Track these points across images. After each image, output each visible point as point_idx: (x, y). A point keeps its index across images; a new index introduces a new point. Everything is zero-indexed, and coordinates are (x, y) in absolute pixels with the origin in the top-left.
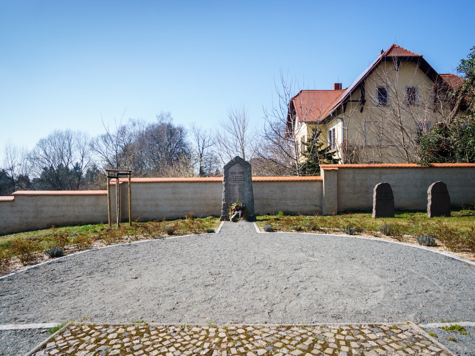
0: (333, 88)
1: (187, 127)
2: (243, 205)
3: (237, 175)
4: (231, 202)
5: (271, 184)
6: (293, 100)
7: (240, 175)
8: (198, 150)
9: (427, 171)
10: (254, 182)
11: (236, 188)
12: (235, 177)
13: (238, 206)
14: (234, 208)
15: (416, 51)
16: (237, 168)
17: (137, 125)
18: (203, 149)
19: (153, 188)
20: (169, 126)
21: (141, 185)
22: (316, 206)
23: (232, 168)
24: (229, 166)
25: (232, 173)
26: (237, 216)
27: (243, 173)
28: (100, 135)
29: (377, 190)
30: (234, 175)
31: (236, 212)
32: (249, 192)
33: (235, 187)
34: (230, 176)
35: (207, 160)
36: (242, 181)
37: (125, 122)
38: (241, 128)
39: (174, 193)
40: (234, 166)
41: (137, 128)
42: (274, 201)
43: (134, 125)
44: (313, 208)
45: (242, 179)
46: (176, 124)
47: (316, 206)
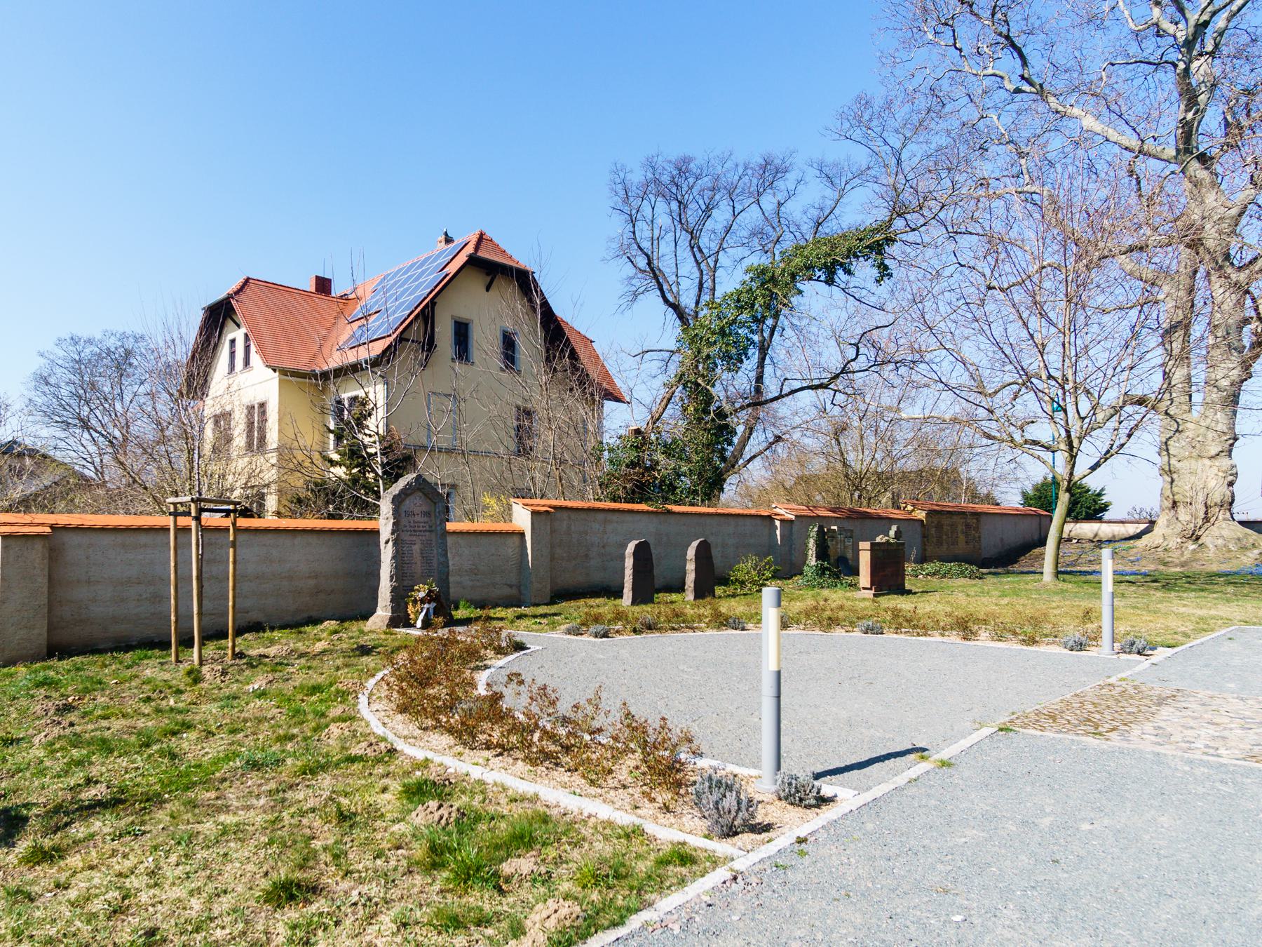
0: (310, 286)
3: (418, 518)
9: (662, 518)
15: (521, 257)
16: (418, 502)
19: (145, 546)
21: (107, 539)
22: (511, 586)
27: (428, 514)
29: (634, 554)
34: (404, 521)
40: (412, 497)
44: (507, 591)
47: (511, 586)
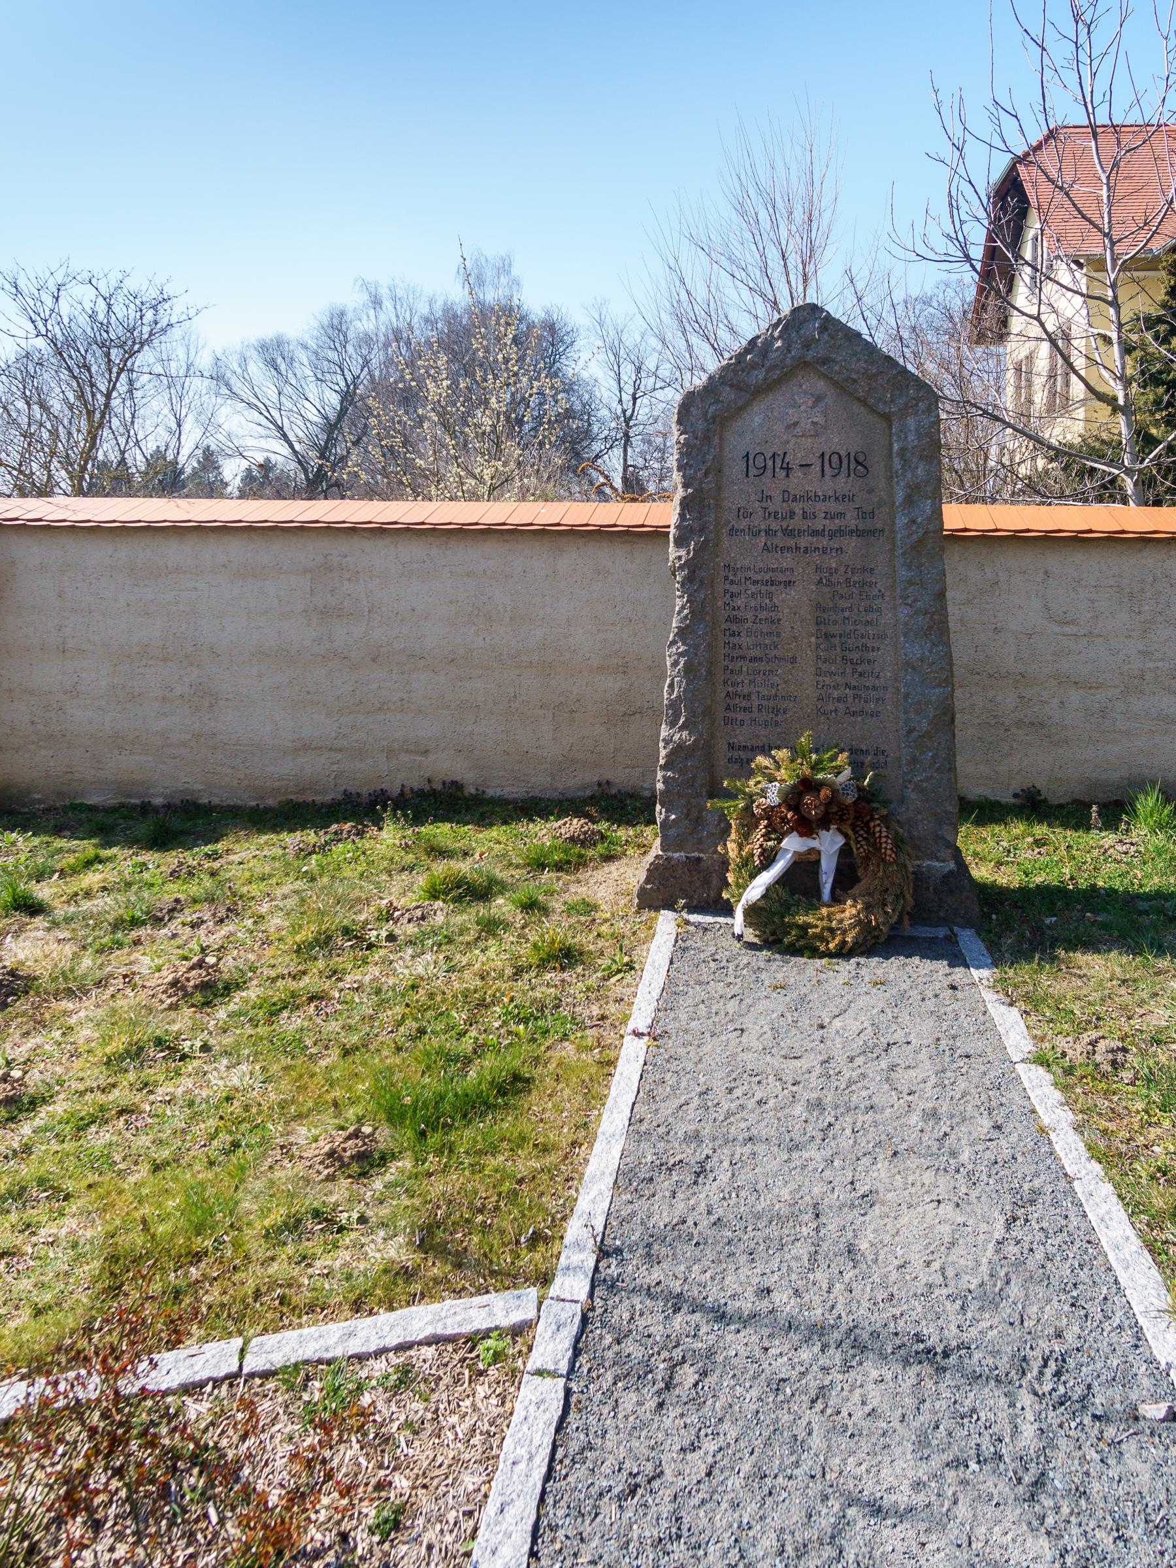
1: (575, 315)
2: (858, 775)
3: (799, 482)
4: (741, 736)
5: (1054, 561)
6: (1021, 168)
7: (827, 486)
8: (615, 405)
10: (959, 538)
11: (795, 603)
12: (786, 496)
13: (807, 785)
14: (773, 797)
17: (388, 304)
18: (635, 399)
19: (177, 569)
20: (508, 312)
21: (98, 552)
23: (756, 417)
24: (728, 394)
25: (760, 465)
26: (800, 881)
28: (253, 341)
30: (774, 485)
31: (792, 844)
32: (915, 650)
33: (783, 597)
34: (739, 492)
35: (650, 442)
36: (851, 544)
37: (353, 300)
38: (794, 260)
39: (324, 613)
40: (777, 401)
41: (388, 316)
42: (1075, 697)
43: (377, 303)
45: (851, 520)
46: (535, 302)
